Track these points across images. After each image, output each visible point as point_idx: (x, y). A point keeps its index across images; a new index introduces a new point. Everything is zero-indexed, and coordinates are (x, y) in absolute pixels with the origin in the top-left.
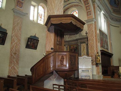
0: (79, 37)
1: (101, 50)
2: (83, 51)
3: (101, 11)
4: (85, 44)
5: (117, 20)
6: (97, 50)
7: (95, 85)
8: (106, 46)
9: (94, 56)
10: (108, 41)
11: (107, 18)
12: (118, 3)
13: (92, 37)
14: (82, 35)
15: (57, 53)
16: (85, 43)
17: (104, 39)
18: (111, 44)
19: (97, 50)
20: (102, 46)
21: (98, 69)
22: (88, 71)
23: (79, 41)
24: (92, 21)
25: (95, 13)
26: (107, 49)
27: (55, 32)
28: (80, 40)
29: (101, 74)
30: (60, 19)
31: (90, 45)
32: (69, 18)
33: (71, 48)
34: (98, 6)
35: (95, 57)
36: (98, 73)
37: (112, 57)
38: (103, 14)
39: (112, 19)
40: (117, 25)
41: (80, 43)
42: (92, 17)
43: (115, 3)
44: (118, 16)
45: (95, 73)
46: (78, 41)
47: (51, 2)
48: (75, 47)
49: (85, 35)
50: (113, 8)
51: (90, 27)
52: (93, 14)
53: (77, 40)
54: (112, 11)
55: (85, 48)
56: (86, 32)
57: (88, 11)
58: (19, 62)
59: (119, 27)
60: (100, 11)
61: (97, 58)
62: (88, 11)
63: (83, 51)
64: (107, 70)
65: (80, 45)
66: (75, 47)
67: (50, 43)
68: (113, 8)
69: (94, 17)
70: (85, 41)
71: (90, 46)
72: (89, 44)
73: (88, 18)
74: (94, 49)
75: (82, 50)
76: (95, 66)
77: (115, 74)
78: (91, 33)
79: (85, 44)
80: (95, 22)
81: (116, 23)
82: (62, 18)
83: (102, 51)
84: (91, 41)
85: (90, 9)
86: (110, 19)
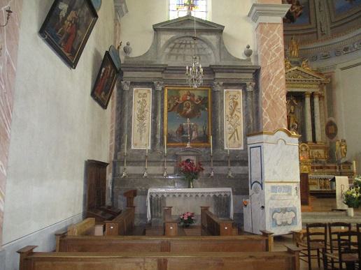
0: (218, 61)
2: (232, 115)
4: (137, 91)
13: (276, 70)
14: (233, 54)
22: (289, 189)
23: (218, 75)
28: (224, 74)
31: (268, 96)
33: (178, 98)
41: (131, 83)
46: (214, 73)
48: (196, 98)
49: (244, 58)
51: (269, 32)
53: (212, 69)
56: (248, 47)
58: (8, 131)
63: (232, 115)
65: (130, 91)
66: (196, 98)
70: (243, 81)
71: (269, 102)
75: (227, 110)
78: (274, 55)
79: (239, 93)
84: (271, 84)
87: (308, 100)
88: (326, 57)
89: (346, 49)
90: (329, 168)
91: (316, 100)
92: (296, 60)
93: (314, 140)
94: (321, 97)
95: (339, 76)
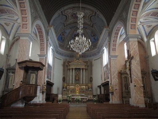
1: (47, 81)
3: (51, 46)
5: (61, 54)
6: (44, 81)
7: (14, 117)
8: (50, 77)
9: (42, 86)
10: (52, 72)
11: (54, 52)
12: (64, 40)
15: (27, 85)
16: (35, 73)
17: (50, 70)
18: (53, 74)
19: (44, 81)
20: (48, 77)
21: (43, 96)
24: (44, 56)
25: (47, 50)
26: (50, 79)
27: (24, 69)
29: (44, 100)
30: (33, 63)
31: (39, 76)
32: (38, 64)
34: (50, 44)
35: (42, 86)
36: (43, 99)
37: (52, 86)
38: (52, 49)
39: (57, 52)
40: (60, 58)
42: (44, 53)
43: (62, 39)
44: (62, 50)
45: (116, 101)
47: (23, 46)
50: (60, 43)
52: (46, 51)
54: (58, 46)
55: (34, 78)
57: (41, 47)
59: (61, 60)
60: (50, 46)
61: (44, 87)
62: (41, 47)
64: (50, 97)
65: (30, 75)
67: (19, 77)
68: (60, 43)
69: (45, 54)
71: (39, 77)
72: (38, 75)
73: (41, 53)
74: (42, 80)
75: (31, 79)
76: (41, 93)
77: (55, 100)
80: (46, 58)
81: (59, 56)
82: (34, 63)
83: (47, 82)
85: (44, 46)
86: (56, 53)
87: (81, 70)
88: (90, 56)
89: (95, 54)
90: (85, 92)
91: (84, 70)
92: (78, 58)
93: (83, 83)
94: (86, 69)
95: (94, 62)
